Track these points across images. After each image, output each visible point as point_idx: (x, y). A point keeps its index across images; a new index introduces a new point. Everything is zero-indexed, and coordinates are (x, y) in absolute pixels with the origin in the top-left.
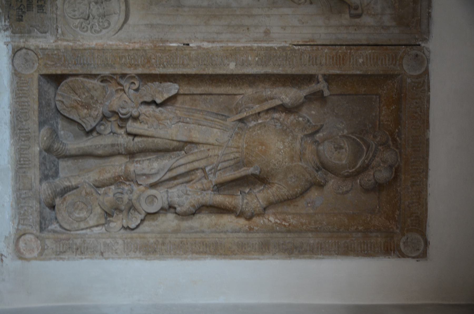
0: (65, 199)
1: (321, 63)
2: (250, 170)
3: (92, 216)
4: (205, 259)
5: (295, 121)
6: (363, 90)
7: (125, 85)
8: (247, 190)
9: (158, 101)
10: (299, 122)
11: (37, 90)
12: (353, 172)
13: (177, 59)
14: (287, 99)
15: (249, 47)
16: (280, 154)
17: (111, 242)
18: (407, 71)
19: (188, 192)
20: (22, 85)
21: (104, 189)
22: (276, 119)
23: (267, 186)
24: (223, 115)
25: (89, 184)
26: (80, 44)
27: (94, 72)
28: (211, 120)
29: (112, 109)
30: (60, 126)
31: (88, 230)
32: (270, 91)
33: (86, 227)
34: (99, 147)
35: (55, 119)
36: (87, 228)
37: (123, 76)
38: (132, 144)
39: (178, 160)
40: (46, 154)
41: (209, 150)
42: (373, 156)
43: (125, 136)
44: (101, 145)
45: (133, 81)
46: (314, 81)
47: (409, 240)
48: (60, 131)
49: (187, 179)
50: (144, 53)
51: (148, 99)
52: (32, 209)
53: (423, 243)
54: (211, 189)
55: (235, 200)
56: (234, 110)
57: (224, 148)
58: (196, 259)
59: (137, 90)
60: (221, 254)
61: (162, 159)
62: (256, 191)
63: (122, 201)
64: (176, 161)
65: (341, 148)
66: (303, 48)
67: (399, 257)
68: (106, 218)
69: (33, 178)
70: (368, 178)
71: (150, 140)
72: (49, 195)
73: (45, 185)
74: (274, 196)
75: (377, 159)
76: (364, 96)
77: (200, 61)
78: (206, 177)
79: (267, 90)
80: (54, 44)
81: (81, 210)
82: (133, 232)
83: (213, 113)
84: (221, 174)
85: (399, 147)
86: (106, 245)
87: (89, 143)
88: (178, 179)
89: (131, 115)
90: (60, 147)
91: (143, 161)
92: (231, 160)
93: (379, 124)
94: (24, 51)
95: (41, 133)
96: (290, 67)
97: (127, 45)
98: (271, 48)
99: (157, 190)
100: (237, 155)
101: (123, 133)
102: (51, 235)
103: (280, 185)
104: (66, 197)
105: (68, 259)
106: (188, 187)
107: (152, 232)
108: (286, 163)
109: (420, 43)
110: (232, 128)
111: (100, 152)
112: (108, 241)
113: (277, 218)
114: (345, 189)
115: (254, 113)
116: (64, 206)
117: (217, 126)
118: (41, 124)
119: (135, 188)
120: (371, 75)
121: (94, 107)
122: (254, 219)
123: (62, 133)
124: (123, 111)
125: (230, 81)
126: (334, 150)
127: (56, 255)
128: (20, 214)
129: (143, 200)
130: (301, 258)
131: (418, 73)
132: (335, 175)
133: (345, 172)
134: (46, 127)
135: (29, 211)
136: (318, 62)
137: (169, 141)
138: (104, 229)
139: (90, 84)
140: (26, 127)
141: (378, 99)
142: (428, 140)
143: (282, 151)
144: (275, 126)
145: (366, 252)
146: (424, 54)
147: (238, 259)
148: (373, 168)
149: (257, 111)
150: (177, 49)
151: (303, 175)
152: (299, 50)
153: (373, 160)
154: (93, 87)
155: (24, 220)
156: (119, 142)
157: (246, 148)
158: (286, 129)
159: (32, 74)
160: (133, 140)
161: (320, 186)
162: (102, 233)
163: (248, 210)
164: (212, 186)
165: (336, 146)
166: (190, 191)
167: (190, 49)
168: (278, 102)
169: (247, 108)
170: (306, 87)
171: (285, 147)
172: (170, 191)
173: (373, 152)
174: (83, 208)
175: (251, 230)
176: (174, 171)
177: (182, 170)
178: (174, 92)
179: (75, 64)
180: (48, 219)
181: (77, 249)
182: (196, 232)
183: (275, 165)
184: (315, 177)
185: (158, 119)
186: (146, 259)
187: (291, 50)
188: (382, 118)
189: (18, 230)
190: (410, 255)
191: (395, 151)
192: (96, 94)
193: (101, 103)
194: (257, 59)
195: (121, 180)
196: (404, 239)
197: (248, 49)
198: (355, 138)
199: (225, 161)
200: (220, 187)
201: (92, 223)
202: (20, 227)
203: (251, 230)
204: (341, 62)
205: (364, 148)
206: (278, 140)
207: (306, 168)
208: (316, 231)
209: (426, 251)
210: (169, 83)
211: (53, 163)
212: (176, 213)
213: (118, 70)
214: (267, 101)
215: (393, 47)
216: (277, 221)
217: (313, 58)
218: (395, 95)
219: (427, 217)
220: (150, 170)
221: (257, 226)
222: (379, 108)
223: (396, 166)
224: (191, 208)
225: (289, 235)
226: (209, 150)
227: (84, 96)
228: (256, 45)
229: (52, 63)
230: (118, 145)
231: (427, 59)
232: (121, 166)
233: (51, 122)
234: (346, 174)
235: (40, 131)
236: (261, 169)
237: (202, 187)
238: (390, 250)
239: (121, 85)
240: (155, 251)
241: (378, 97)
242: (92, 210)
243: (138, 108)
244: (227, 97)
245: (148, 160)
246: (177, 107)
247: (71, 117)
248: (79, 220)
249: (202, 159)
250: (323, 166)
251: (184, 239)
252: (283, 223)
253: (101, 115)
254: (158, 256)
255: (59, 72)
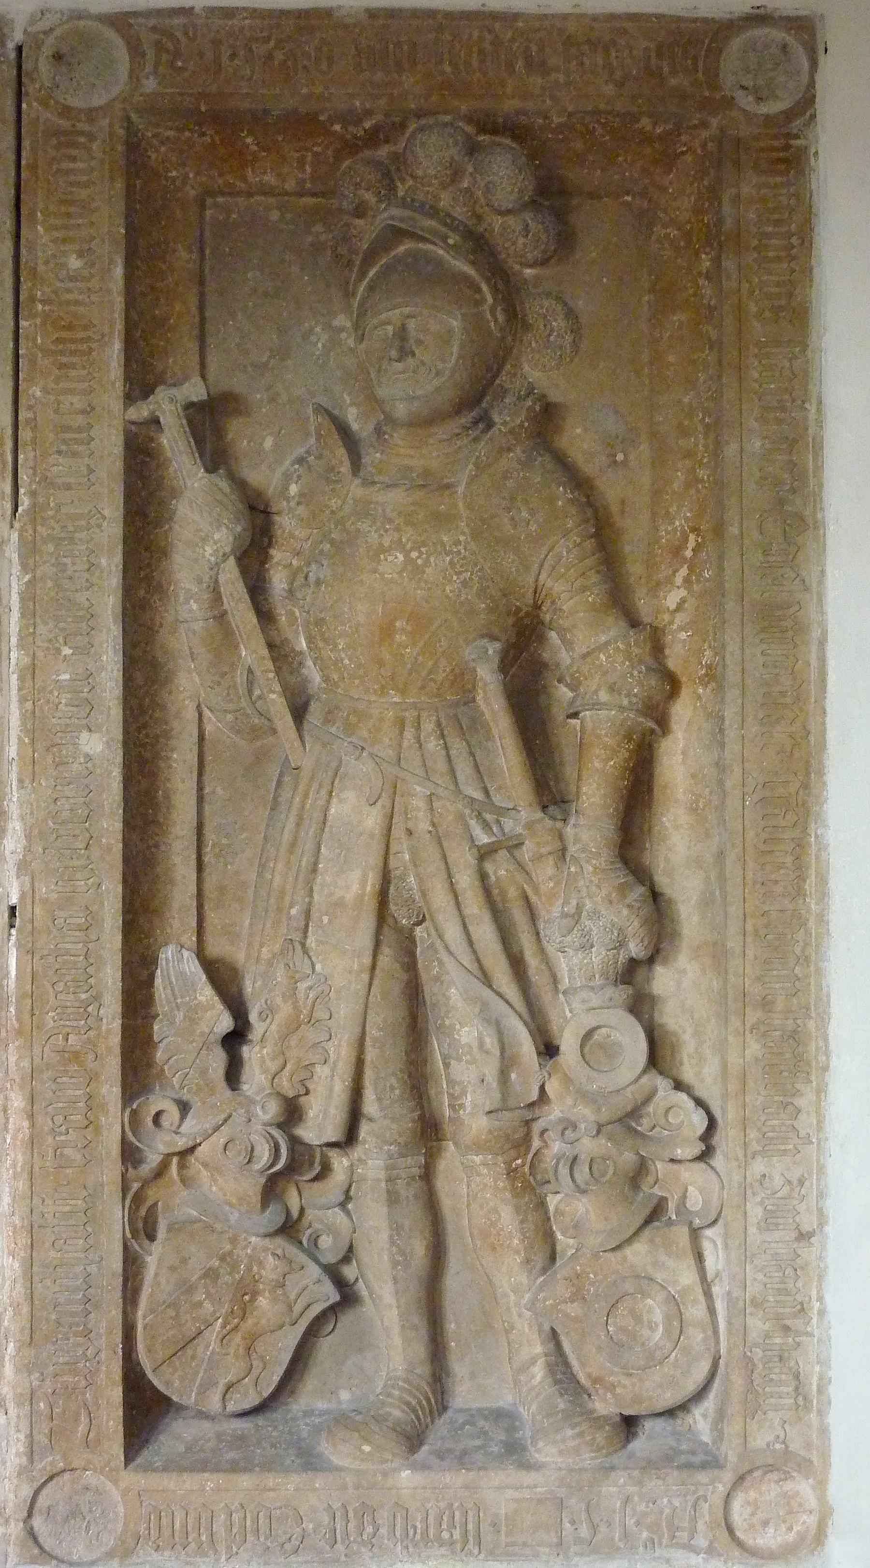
0: (596, 1381)
1: (83, 412)
2: (488, 678)
3: (659, 1277)
4: (822, 847)
5: (301, 509)
6: (184, 255)
7: (163, 1149)
8: (564, 693)
9: (226, 1023)
10: (304, 497)
11: (185, 1476)
12: (495, 290)
13: (67, 953)
14: (216, 536)
15: (22, 679)
16: (427, 563)
17: (762, 1202)
18: (116, 91)
19: (570, 909)
20: (166, 1533)
21: (559, 1236)
22: (291, 582)
23: (547, 618)
24: (279, 784)
25: (541, 1288)
26: (9, 1313)
27: (117, 1265)
28: (298, 825)
29: (255, 1196)
30: (321, 1405)
31: (716, 1290)
32: (187, 602)
33: (701, 1298)
34: (402, 1252)
35: (294, 1419)
36: (708, 1295)
37: (130, 1155)
38: (387, 1122)
39: (447, 948)
40: (425, 1448)
41: (410, 832)
42: (432, 217)
43: (357, 1152)
44: (392, 1243)
45: (149, 1120)
46: (152, 440)
47: (749, 83)
48: (340, 1402)
49: (518, 915)
50: (45, 1076)
51: (218, 1060)
52: (636, 1498)
53: (759, 32)
54: (559, 824)
55: (598, 737)
56: (259, 743)
57: (402, 774)
58: (823, 880)
59: (184, 1107)
60: (806, 786)
61: (443, 1010)
62: (564, 657)
63: (604, 1159)
64: (451, 953)
65: (402, 334)
66: (24, 477)
67: (813, 117)
68: (670, 1223)
69: (517, 1495)
70: (518, 236)
71: (371, 1055)
72: (581, 1434)
73: (545, 1453)
74: (584, 589)
75: (445, 201)
76: (207, 251)
77: (76, 863)
78: (514, 846)
79: (183, 615)
80: (13, 1411)
81: (638, 1318)
82: (720, 1120)
83: (271, 818)
84: (500, 788)
85: (397, 120)
86: (769, 1222)
87: (386, 1292)
88: (521, 952)
89: (280, 1126)
90: (400, 1399)
91: (451, 1083)
92: (446, 748)
93: (314, 195)
94: (37, 1522)
95: (345, 1462)
96: (99, 526)
97: (14, 1138)
98: (29, 597)
99: (561, 1031)
100: (428, 726)
101: (345, 1162)
102: (732, 1428)
103: (541, 565)
104: (589, 1376)
105: (824, 1362)
106: (552, 913)
107: (722, 1047)
108: (457, 543)
109: (11, 45)
110: (324, 745)
111: (419, 1248)
112: (755, 1212)
113: (670, 580)
114: (559, 323)
115: (270, 665)
116: (625, 1381)
117: (321, 803)
118: (310, 1461)
119: (554, 1113)
120: (130, 228)
121: (249, 1268)
122: (672, 664)
123: (345, 1395)
124: (264, 1154)
125: (148, 755)
126: (410, 360)
127: (808, 1408)
128: (650, 1544)
129: (598, 1083)
130: (821, 486)
131: (122, 53)
132: (504, 360)
133: (495, 320)
134: (324, 1447)
135: (642, 1507)
136: (80, 420)
137: (376, 982)
138: (708, 1232)
139: (163, 1280)
140: (326, 1519)
141: (220, 199)
142: (373, 14)
143: (414, 554)
144: (318, 583)
145: (794, 240)
146: (52, 30)
147: (824, 724)
148: (479, 218)
149: (265, 652)
150: (28, 951)
151: (505, 478)
152: (33, 494)
153: (448, 215)
154: (172, 1269)
155: (673, 1529)
156: (382, 1175)
157: (403, 692)
158: (332, 542)
159: (125, 1493)
160: (370, 1120)
161: (546, 418)
162: (726, 1236)
163: (638, 684)
164: (549, 823)
165: (394, 353)
166: (566, 903)
167: (29, 901)
168: (230, 577)
169: (250, 692)
170: (171, 469)
171: (399, 545)
172: (565, 983)
173: (417, 216)
174: (632, 1313)
175: (713, 676)
176: (488, 963)
177: (485, 933)
178: (192, 966)
179: (87, 1333)
180: (674, 1444)
181: (786, 1329)
182: (722, 879)
183: (465, 583)
184: (511, 432)
185: (294, 1026)
186: (826, 1068)
187: (34, 522)
188: (290, 185)
189: (711, 1551)
190: (805, 79)
191: (414, 133)
192: (199, 1259)
193: (234, 1241)
194: (67, 651)
195: (526, 1169)
196: (745, 101)
197: (29, 683)
198: (365, 283)
199: (452, 772)
200: (550, 791)
201: (688, 1277)
202: (702, 1542)
203: (713, 676)
204: (81, 334)
205: (402, 249)
206: (375, 571)
207: (477, 466)
208: (715, 428)
209: (788, 19)
210: (158, 981)
211: (461, 1428)
212: (651, 960)
213: (110, 1171)
214: (224, 614)
215: (26, 144)
216: (679, 580)
217: (64, 441)
218: (204, 134)
219: (659, 17)
220: (487, 1052)
221: (701, 651)
222: (250, 195)
223: (469, 129)
224: (628, 901)
225: (734, 531)
226: (410, 832)
227: (208, 1306)
228: (14, 655)
229: (84, 1418)
230: (390, 1180)
231: (71, 18)
232: (470, 1169)
233: (305, 1435)
234: (501, 317)
235: (339, 1469)
236: (482, 636)
237: (551, 861)
238: (784, 151)
239: (164, 1166)
240: (795, 1036)
241: (209, 201)
242: (637, 1277)
243: (252, 1102)
244: (207, 769)
245: (447, 1065)
246: (248, 956)
247: (286, 1358)
248: (676, 1324)
249: (445, 857)
250: (474, 401)
251: (749, 928)
252: (688, 553)
253: (280, 1241)
254: (811, 1025)
255: (117, 1394)
